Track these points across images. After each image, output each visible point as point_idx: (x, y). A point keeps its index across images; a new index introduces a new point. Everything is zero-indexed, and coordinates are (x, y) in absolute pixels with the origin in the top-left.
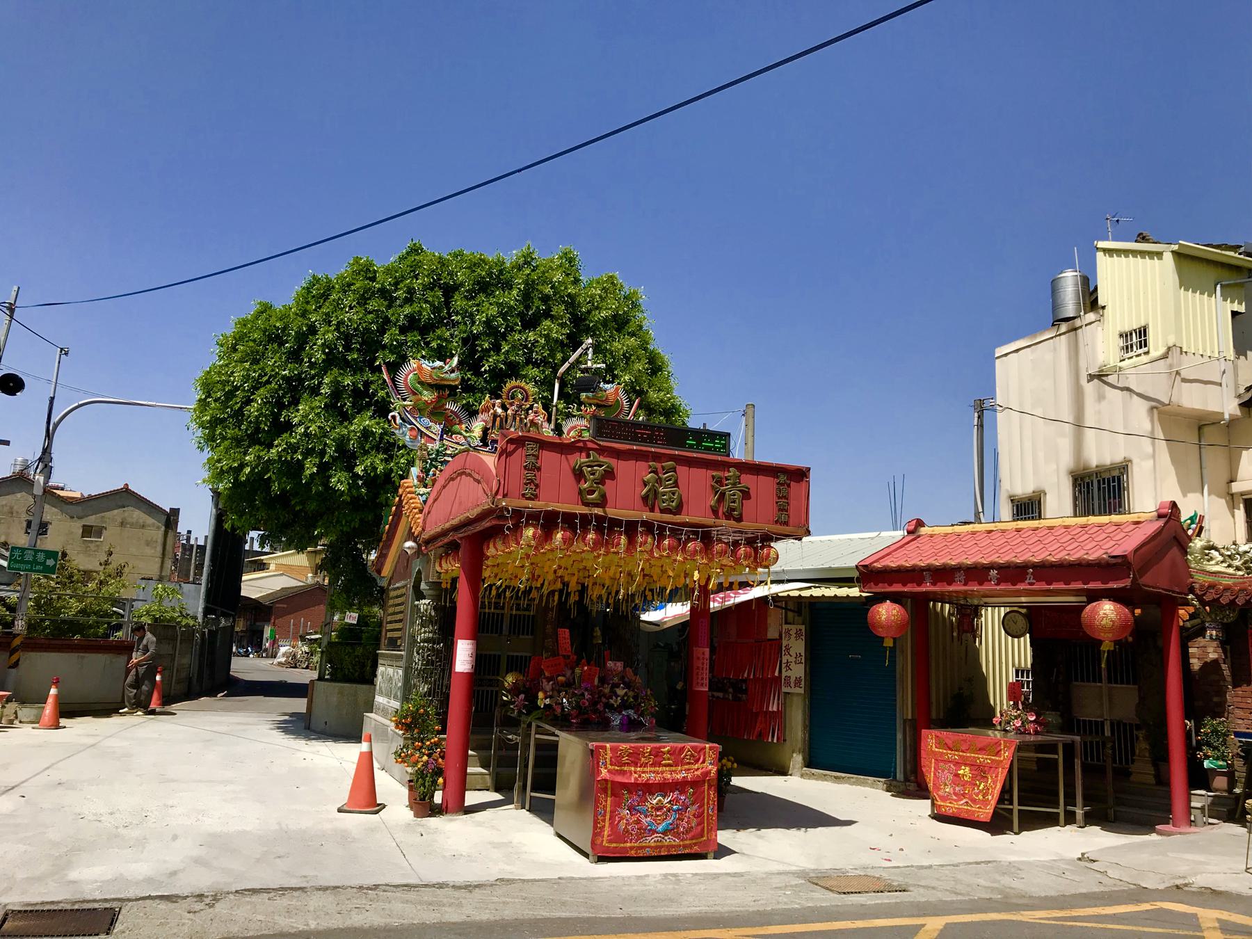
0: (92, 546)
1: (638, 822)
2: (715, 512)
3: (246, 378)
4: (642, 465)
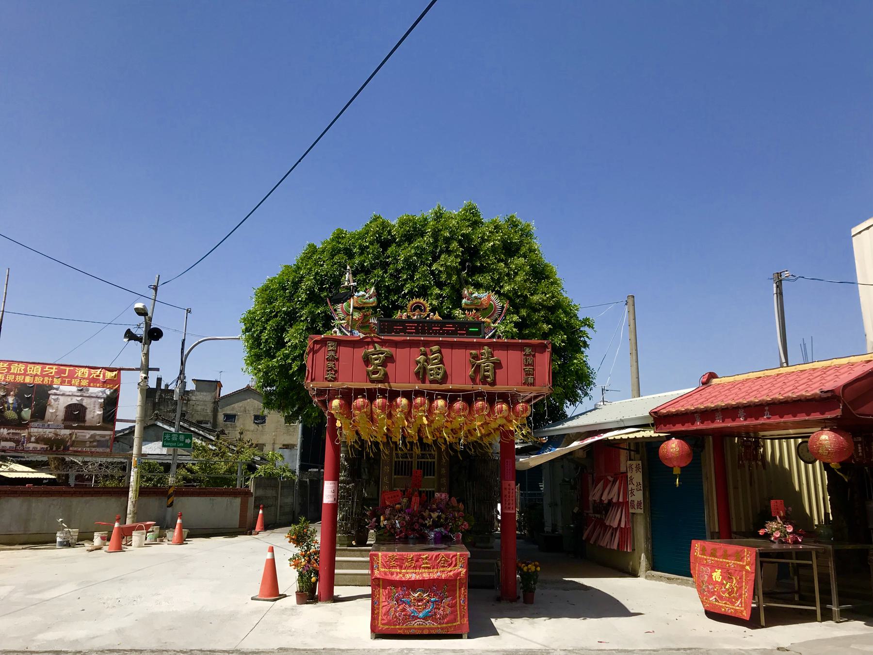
0: (291, 429)
1: (404, 610)
2: (473, 380)
3: (264, 314)
4: (414, 350)
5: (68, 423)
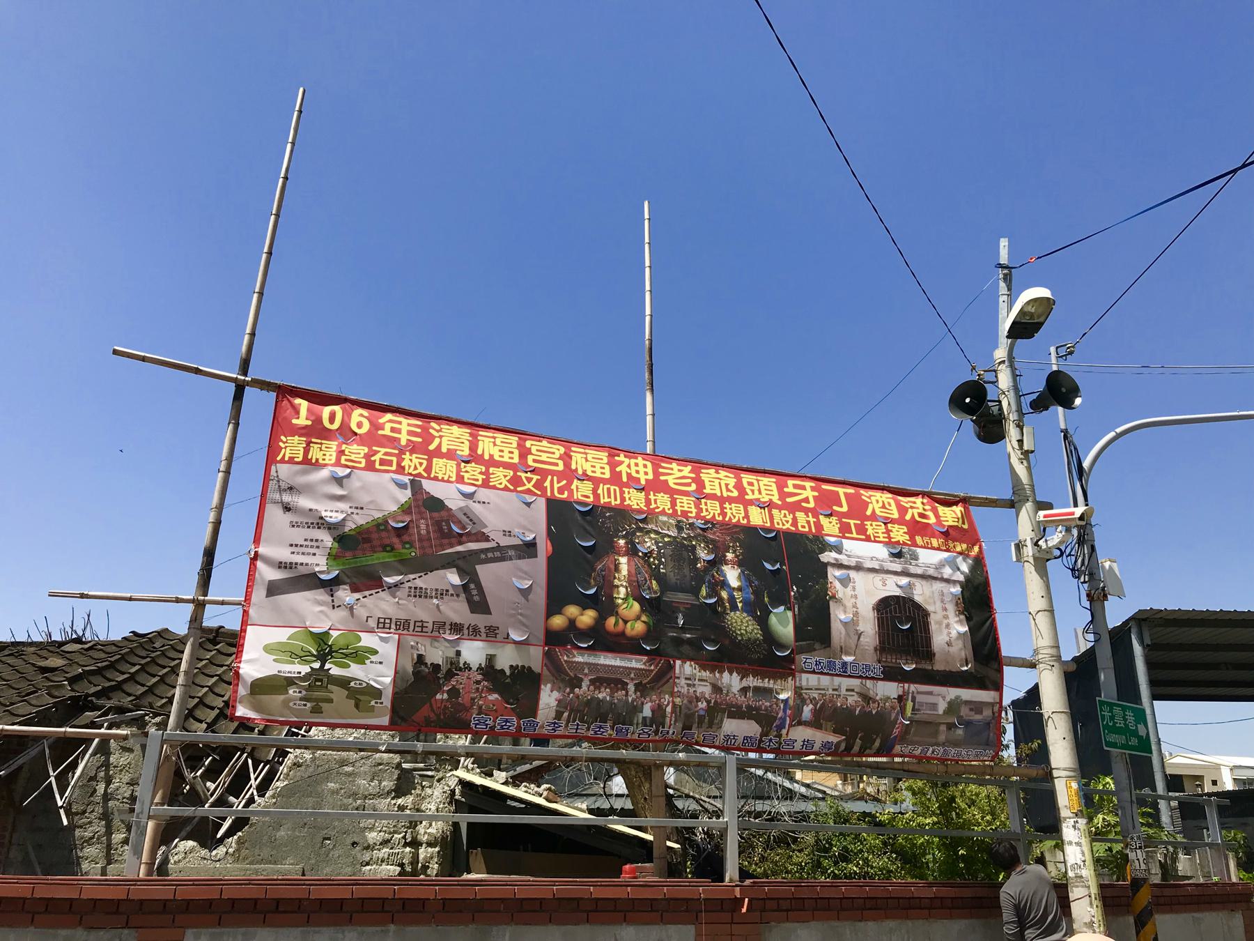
5: (891, 660)
